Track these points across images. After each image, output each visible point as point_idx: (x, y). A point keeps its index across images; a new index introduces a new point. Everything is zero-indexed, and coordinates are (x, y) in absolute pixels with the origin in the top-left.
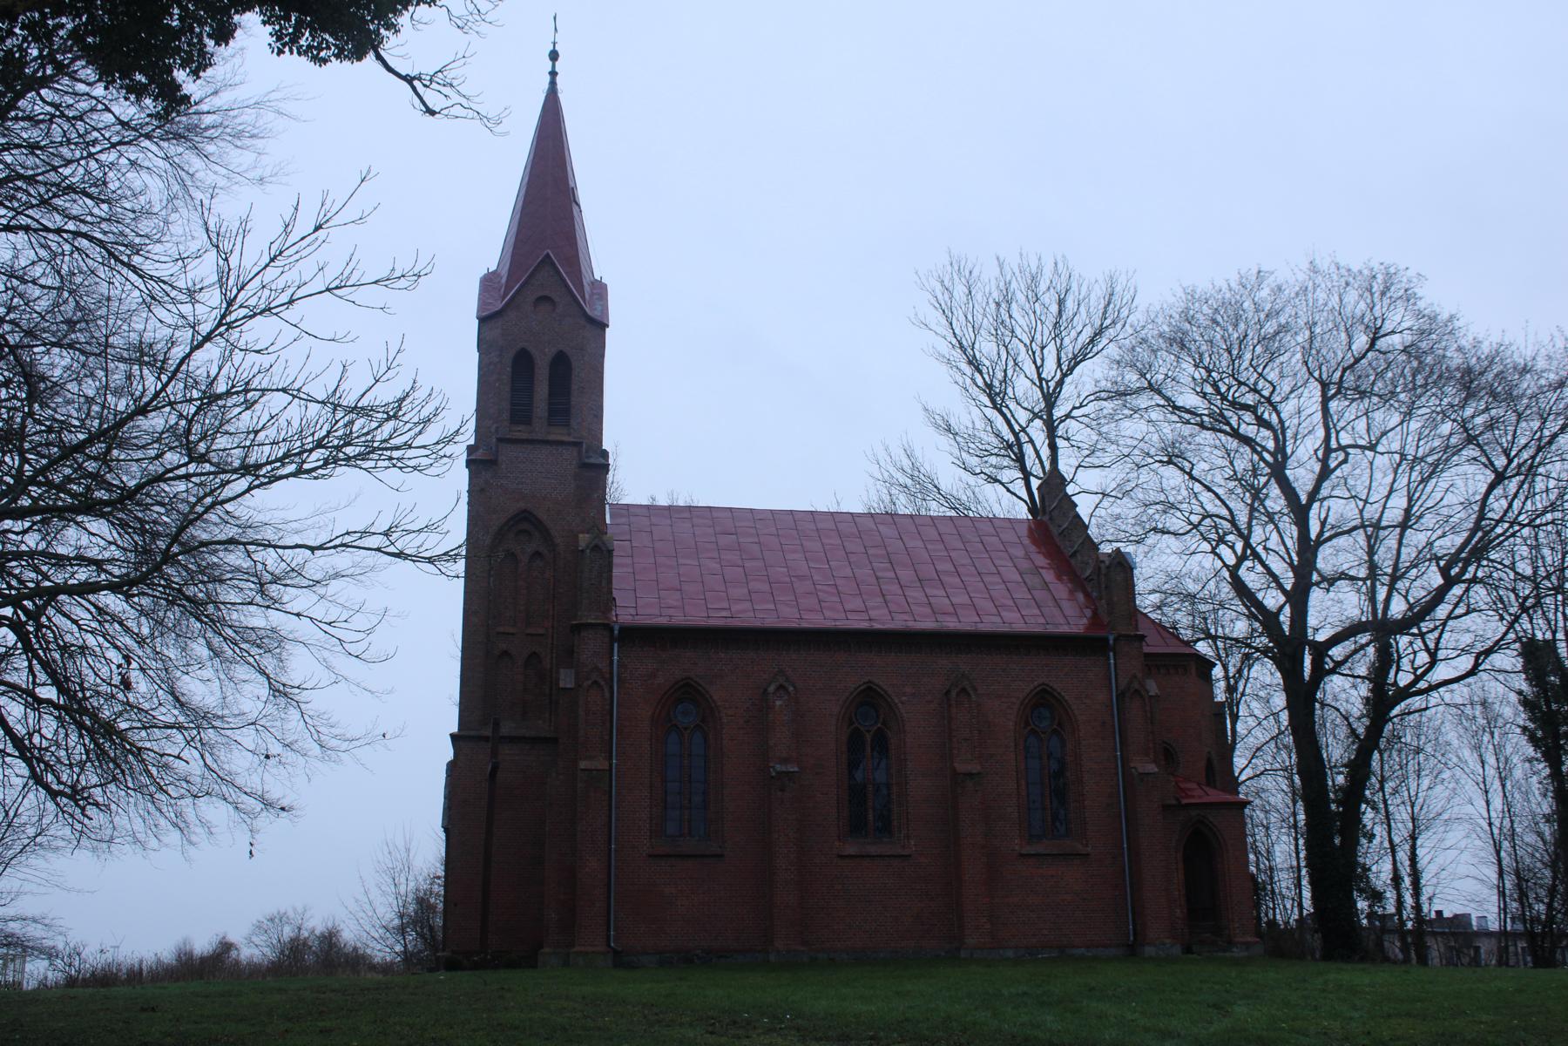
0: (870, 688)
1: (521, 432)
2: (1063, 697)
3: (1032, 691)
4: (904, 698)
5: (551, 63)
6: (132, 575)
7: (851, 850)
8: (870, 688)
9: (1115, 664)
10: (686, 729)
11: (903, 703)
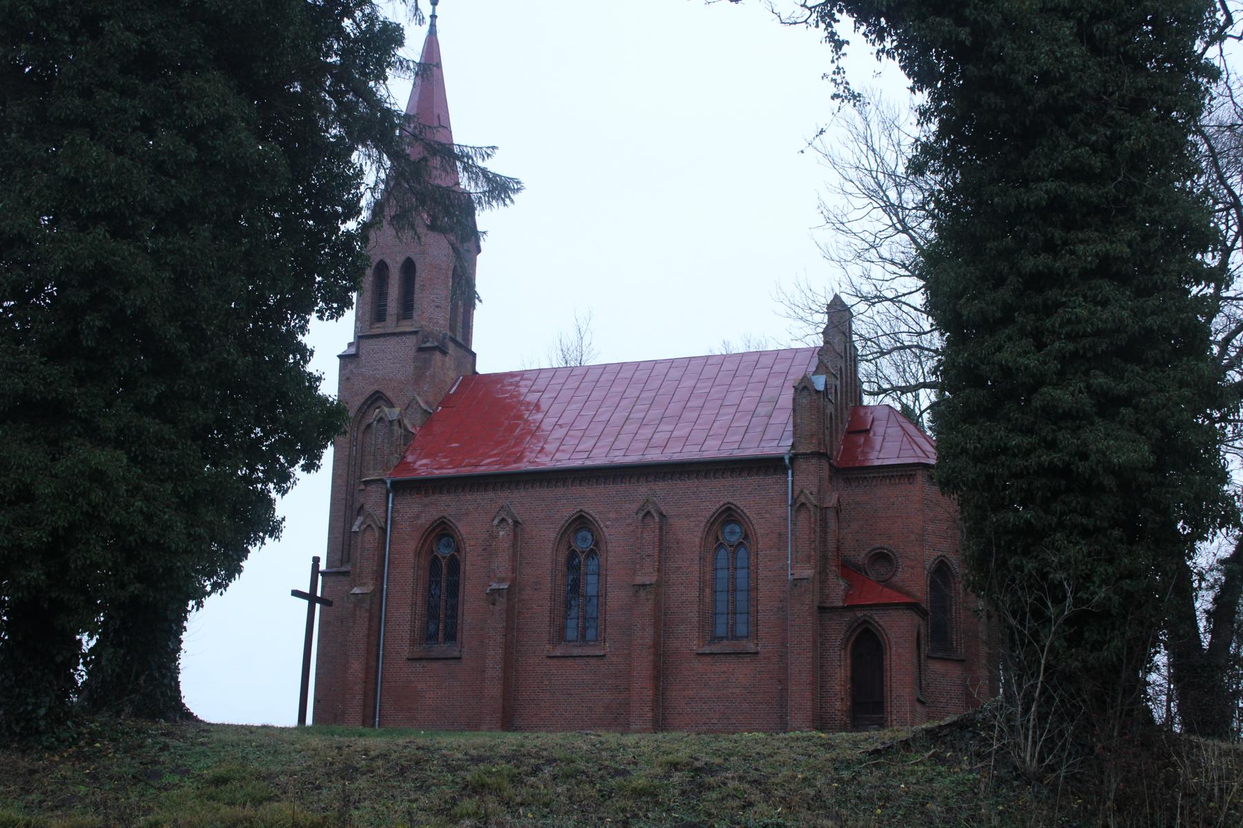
0: (581, 516)
1: (379, 329)
2: (745, 514)
3: (717, 510)
4: (608, 523)
5: (431, 7)
6: (1205, 80)
7: (559, 652)
8: (581, 516)
9: (793, 482)
10: (583, 552)
11: (607, 527)
